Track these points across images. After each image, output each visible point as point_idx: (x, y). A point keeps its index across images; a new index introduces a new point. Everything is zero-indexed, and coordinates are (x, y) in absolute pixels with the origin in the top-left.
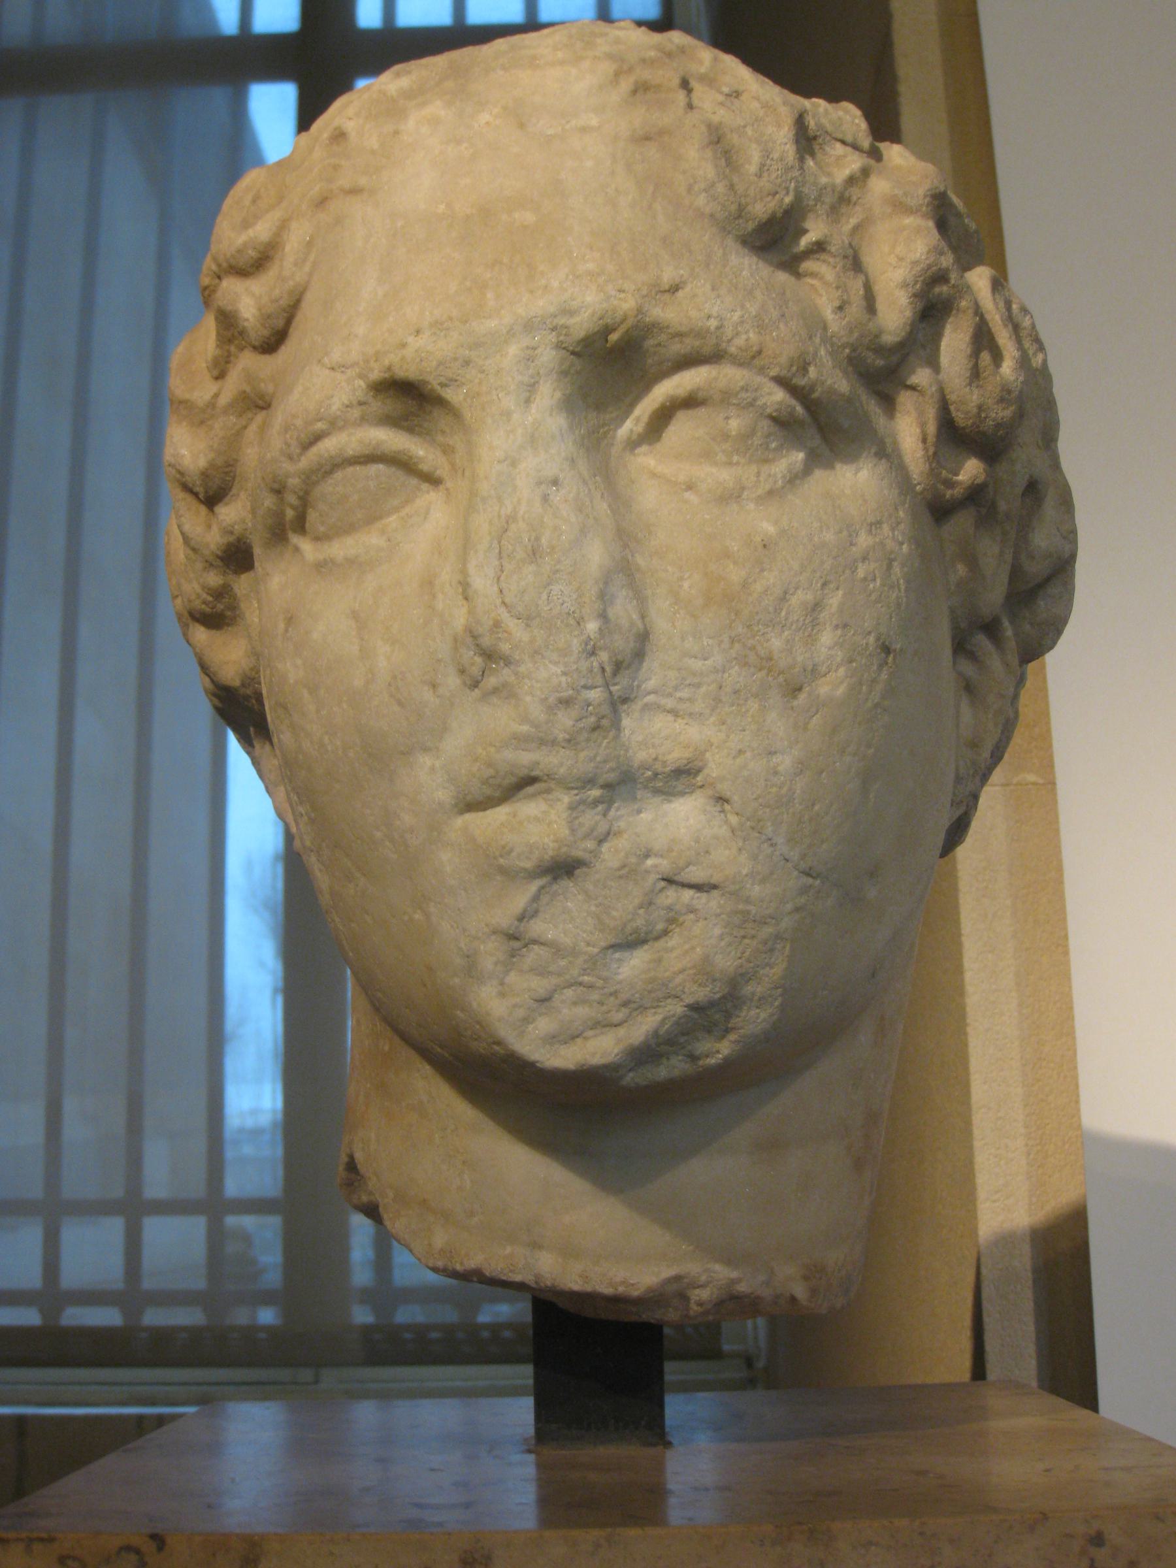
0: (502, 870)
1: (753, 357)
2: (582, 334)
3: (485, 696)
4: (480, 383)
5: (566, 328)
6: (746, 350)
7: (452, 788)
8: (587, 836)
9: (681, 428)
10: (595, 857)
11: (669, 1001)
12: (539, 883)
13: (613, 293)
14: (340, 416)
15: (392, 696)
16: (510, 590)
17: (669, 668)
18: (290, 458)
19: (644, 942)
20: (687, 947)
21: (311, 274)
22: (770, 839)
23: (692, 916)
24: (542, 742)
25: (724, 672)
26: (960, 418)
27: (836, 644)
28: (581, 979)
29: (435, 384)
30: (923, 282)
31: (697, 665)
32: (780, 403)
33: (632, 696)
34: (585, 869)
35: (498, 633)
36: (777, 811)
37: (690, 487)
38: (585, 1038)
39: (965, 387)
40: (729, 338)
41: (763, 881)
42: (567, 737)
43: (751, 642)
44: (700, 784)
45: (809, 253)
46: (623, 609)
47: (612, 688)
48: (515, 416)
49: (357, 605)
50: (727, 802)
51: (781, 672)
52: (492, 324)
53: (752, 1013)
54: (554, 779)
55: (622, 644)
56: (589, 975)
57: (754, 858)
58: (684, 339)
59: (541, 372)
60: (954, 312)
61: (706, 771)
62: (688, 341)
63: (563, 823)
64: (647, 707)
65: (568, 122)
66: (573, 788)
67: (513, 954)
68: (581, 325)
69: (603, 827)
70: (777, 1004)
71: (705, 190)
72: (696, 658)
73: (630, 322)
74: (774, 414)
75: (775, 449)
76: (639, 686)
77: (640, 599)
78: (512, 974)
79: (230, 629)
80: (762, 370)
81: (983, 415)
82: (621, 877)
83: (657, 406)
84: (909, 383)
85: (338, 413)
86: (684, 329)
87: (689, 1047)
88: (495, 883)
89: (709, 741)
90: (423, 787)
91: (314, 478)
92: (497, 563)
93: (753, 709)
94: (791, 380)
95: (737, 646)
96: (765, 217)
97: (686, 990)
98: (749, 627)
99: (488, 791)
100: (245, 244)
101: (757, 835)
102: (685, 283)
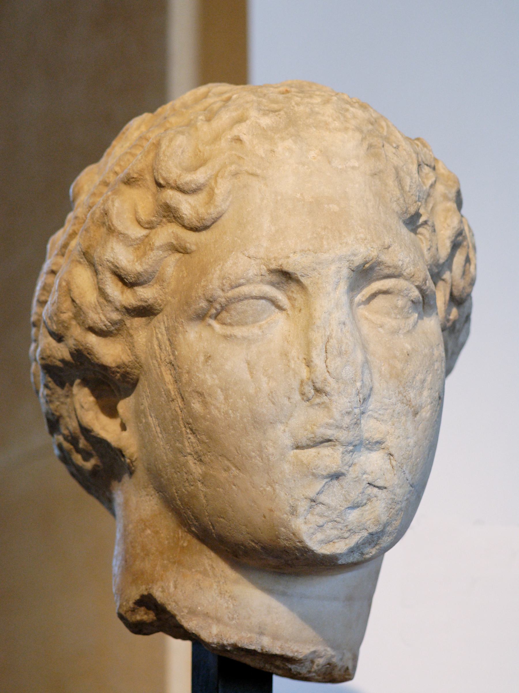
0: (313, 475)
1: (411, 277)
2: (358, 264)
3: (312, 405)
4: (318, 279)
5: (353, 261)
7: (293, 440)
8: (346, 464)
9: (380, 302)
10: (348, 472)
11: (363, 530)
12: (326, 480)
13: (370, 248)
14: (252, 278)
15: (269, 399)
16: (331, 367)
17: (377, 401)
18: (223, 290)
19: (358, 507)
20: (372, 510)
21: (229, 206)
22: (404, 471)
23: (375, 498)
24: (337, 427)
25: (395, 405)
26: (456, 293)
28: (336, 519)
29: (299, 274)
31: (387, 401)
32: (416, 296)
34: (344, 477)
35: (325, 383)
36: (408, 461)
37: (381, 326)
38: (334, 542)
40: (405, 269)
42: (347, 426)
43: (405, 394)
44: (382, 447)
48: (332, 295)
49: (249, 358)
50: (392, 456)
51: (413, 407)
52: (326, 256)
53: (386, 538)
54: (338, 441)
55: (366, 391)
56: (339, 518)
57: (399, 478)
58: (390, 269)
59: (342, 277)
61: (386, 443)
62: (391, 269)
63: (340, 458)
65: (347, 163)
66: (344, 446)
67: (311, 507)
68: (358, 261)
70: (394, 536)
71: (396, 201)
72: (387, 398)
73: (373, 261)
74: (414, 300)
76: (367, 408)
78: (309, 515)
79: (111, 338)
80: (413, 282)
83: (373, 292)
85: (251, 277)
86: (390, 265)
87: (362, 550)
88: (309, 479)
89: (388, 431)
90: (280, 438)
91: (233, 301)
92: (325, 354)
93: (403, 420)
94: (422, 286)
97: (370, 527)
98: (404, 388)
99: (309, 442)
100: (191, 181)
101: (401, 469)
102: (391, 245)
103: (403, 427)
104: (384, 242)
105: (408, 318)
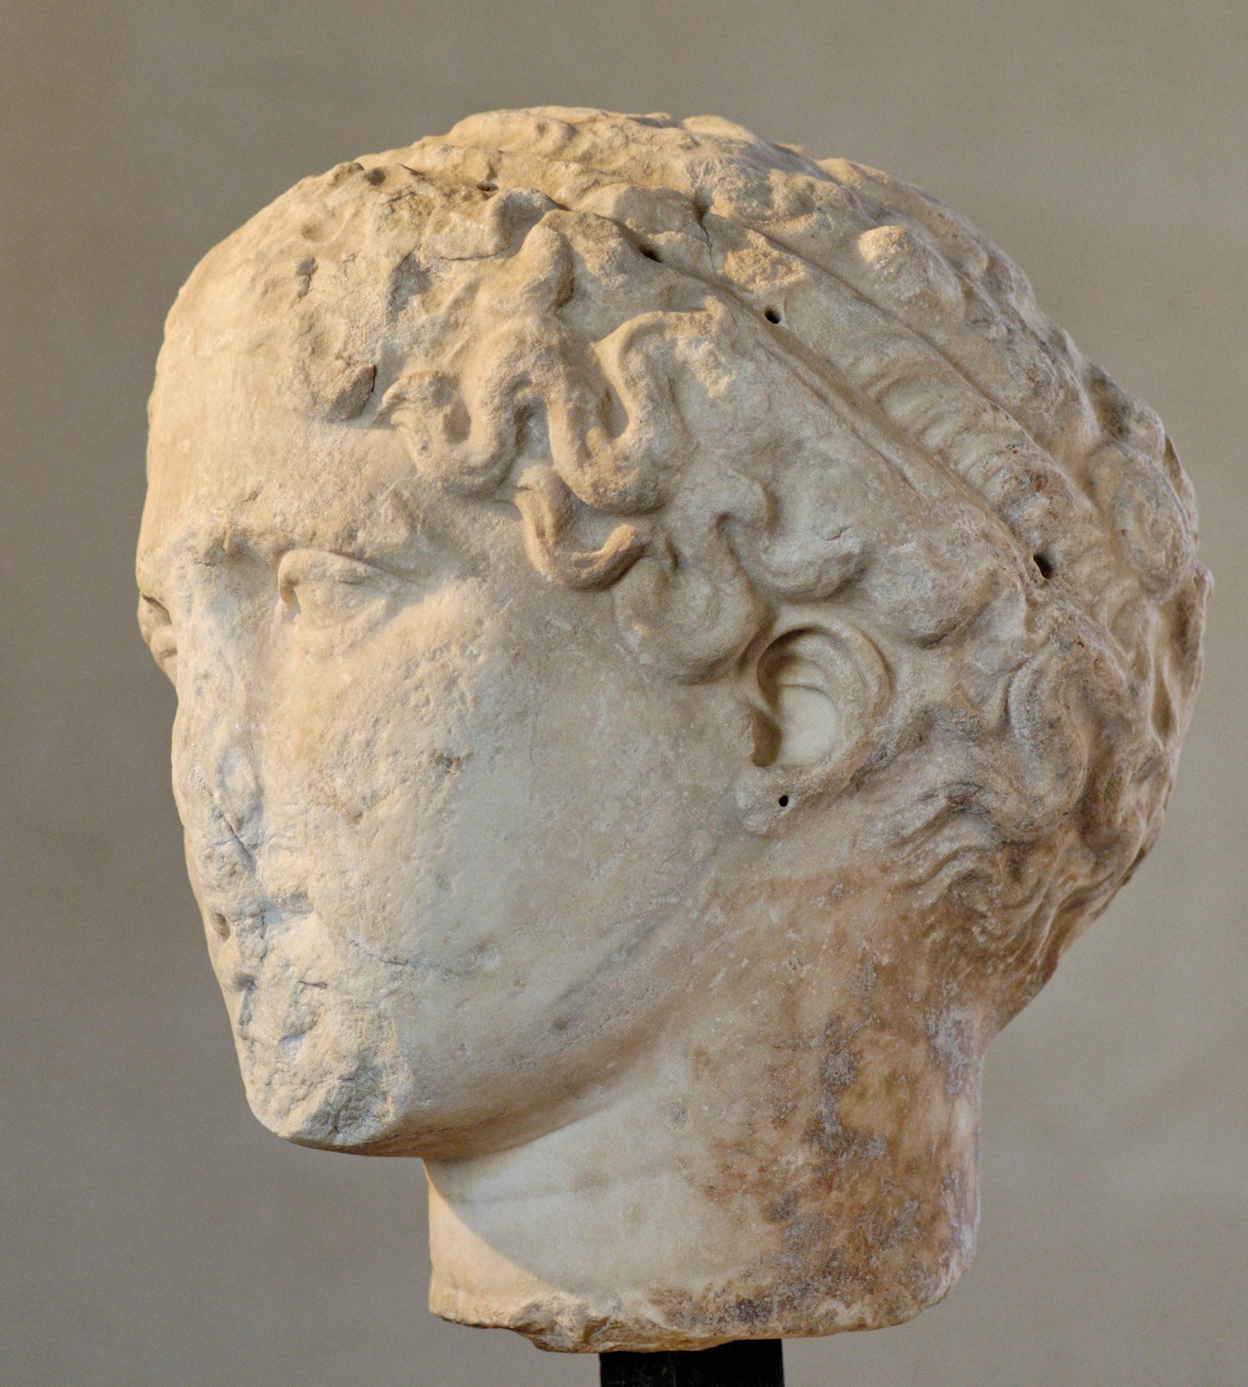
1: (311, 540)
6: (305, 535)
27: (388, 770)
30: (501, 394)
33: (259, 842)
36: (352, 918)
39: (576, 470)
41: (355, 975)
45: (391, 408)
46: (240, 777)
47: (242, 840)
48: (184, 625)
55: (241, 805)
57: (344, 957)
60: (548, 406)
64: (272, 848)
68: (202, 544)
69: (261, 947)
75: (357, 605)
76: (263, 833)
77: (255, 764)
80: (321, 547)
81: (601, 490)
82: (276, 984)
84: (519, 485)
95: (313, 789)
96: (334, 397)
103: (330, 853)
104: (243, 489)
105: (350, 617)
